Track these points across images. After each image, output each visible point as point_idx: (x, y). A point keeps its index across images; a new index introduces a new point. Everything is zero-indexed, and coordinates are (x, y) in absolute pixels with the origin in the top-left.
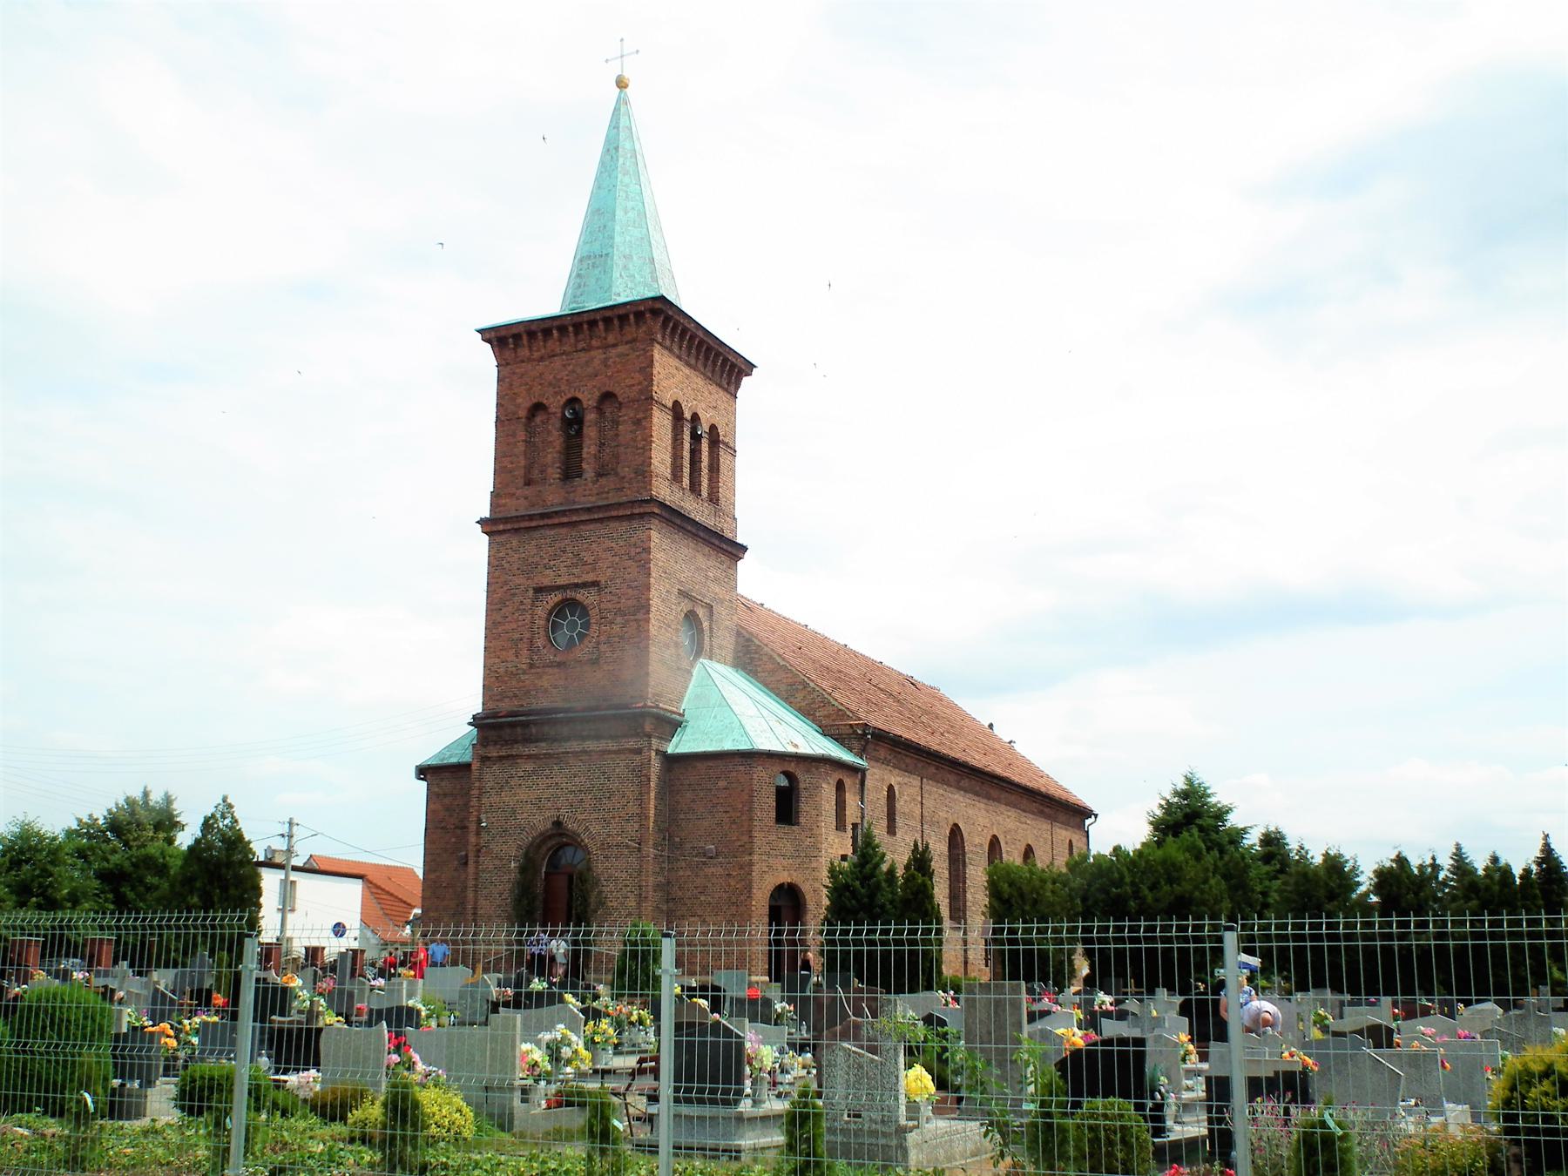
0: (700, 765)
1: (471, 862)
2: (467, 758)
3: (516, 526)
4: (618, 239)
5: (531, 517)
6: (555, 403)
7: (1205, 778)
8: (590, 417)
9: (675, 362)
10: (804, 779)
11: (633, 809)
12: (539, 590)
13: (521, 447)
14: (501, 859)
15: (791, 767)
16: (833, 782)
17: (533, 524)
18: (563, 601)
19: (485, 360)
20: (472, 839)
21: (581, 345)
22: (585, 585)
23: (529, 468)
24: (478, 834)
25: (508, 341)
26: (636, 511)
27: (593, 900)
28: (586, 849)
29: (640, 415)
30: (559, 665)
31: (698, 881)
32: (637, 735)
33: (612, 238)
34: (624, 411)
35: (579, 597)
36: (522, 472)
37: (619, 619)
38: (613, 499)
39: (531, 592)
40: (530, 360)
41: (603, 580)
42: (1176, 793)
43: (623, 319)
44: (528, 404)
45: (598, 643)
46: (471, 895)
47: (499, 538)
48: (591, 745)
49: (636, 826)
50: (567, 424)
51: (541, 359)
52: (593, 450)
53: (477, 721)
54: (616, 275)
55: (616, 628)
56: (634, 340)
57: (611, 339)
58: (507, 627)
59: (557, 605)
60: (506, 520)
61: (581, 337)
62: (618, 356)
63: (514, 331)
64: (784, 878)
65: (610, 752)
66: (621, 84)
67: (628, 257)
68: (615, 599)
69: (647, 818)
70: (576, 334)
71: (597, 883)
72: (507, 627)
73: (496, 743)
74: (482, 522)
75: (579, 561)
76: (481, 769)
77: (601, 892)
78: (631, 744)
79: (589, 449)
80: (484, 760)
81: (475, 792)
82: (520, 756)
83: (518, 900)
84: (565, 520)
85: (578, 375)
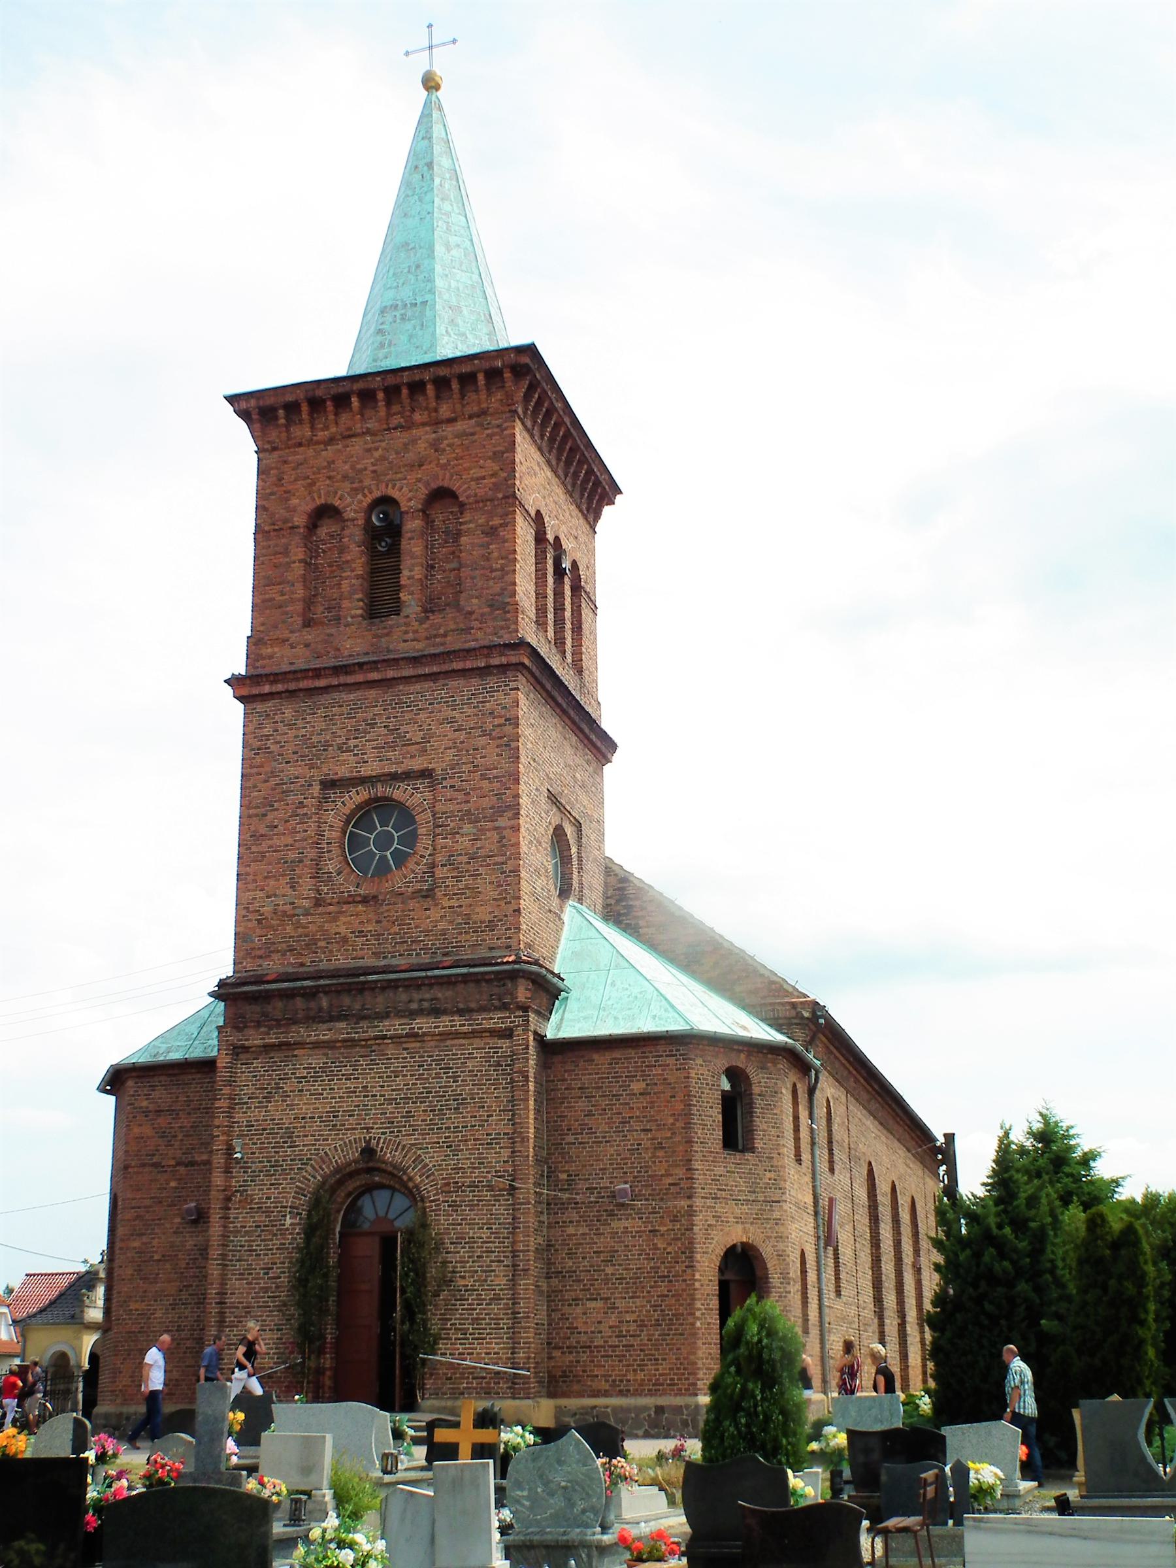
0: (602, 1059)
1: (215, 1218)
2: (208, 1046)
3: (292, 686)
4: (440, 283)
5: (317, 673)
6: (353, 506)
7: (1066, 1116)
8: (412, 525)
9: (537, 455)
10: (759, 1080)
11: (499, 1125)
12: (330, 785)
13: (298, 570)
14: (268, 1212)
15: (740, 1061)
16: (789, 1086)
17: (322, 683)
18: (368, 802)
19: (239, 447)
20: (218, 1179)
21: (396, 420)
22: (407, 776)
23: (309, 602)
24: (227, 1171)
25: (277, 415)
26: (495, 661)
27: (432, 1271)
28: (413, 1195)
29: (496, 521)
30: (365, 900)
31: (601, 1243)
32: (505, 1007)
33: (430, 280)
34: (467, 516)
35: (398, 794)
36: (299, 607)
37: (468, 828)
38: (454, 643)
39: (316, 789)
40: (311, 442)
41: (438, 767)
42: (1031, 1133)
43: (467, 380)
44: (309, 507)
45: (433, 865)
46: (214, 1271)
47: (260, 707)
48: (424, 1024)
49: (505, 1153)
50: (373, 535)
51: (331, 440)
52: (418, 573)
53: (225, 992)
54: (440, 329)
55: (463, 843)
56: (484, 413)
57: (445, 411)
58: (276, 841)
59: (359, 807)
60: (275, 678)
61: (396, 408)
62: (458, 436)
63: (290, 398)
64: (737, 1235)
65: (457, 1035)
66: (430, 83)
67: (456, 309)
68: (460, 796)
69: (525, 1140)
70: (389, 404)
71: (439, 1246)
72: (276, 841)
73: (259, 1024)
74: (233, 682)
75: (397, 739)
76: (231, 1066)
77: (445, 1263)
78: (494, 1021)
79: (411, 571)
80: (238, 1051)
81: (222, 1103)
82: (301, 1045)
83: (301, 1283)
84: (375, 676)
85: (391, 463)
